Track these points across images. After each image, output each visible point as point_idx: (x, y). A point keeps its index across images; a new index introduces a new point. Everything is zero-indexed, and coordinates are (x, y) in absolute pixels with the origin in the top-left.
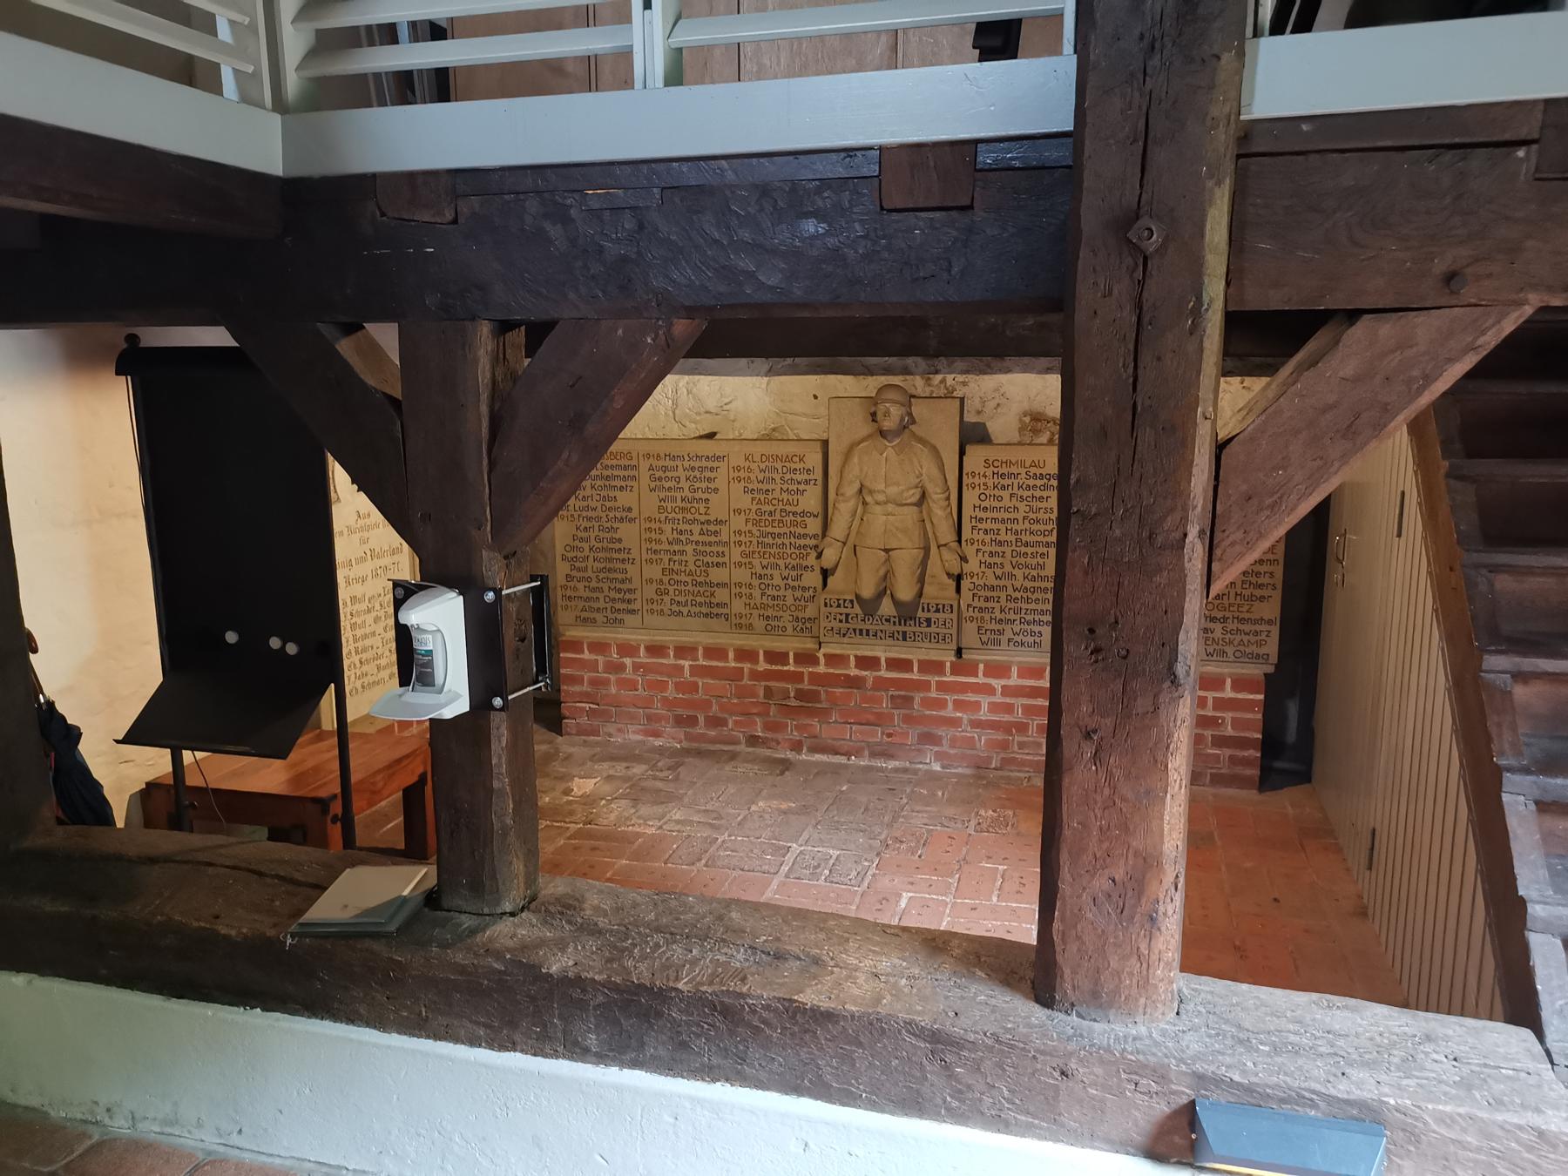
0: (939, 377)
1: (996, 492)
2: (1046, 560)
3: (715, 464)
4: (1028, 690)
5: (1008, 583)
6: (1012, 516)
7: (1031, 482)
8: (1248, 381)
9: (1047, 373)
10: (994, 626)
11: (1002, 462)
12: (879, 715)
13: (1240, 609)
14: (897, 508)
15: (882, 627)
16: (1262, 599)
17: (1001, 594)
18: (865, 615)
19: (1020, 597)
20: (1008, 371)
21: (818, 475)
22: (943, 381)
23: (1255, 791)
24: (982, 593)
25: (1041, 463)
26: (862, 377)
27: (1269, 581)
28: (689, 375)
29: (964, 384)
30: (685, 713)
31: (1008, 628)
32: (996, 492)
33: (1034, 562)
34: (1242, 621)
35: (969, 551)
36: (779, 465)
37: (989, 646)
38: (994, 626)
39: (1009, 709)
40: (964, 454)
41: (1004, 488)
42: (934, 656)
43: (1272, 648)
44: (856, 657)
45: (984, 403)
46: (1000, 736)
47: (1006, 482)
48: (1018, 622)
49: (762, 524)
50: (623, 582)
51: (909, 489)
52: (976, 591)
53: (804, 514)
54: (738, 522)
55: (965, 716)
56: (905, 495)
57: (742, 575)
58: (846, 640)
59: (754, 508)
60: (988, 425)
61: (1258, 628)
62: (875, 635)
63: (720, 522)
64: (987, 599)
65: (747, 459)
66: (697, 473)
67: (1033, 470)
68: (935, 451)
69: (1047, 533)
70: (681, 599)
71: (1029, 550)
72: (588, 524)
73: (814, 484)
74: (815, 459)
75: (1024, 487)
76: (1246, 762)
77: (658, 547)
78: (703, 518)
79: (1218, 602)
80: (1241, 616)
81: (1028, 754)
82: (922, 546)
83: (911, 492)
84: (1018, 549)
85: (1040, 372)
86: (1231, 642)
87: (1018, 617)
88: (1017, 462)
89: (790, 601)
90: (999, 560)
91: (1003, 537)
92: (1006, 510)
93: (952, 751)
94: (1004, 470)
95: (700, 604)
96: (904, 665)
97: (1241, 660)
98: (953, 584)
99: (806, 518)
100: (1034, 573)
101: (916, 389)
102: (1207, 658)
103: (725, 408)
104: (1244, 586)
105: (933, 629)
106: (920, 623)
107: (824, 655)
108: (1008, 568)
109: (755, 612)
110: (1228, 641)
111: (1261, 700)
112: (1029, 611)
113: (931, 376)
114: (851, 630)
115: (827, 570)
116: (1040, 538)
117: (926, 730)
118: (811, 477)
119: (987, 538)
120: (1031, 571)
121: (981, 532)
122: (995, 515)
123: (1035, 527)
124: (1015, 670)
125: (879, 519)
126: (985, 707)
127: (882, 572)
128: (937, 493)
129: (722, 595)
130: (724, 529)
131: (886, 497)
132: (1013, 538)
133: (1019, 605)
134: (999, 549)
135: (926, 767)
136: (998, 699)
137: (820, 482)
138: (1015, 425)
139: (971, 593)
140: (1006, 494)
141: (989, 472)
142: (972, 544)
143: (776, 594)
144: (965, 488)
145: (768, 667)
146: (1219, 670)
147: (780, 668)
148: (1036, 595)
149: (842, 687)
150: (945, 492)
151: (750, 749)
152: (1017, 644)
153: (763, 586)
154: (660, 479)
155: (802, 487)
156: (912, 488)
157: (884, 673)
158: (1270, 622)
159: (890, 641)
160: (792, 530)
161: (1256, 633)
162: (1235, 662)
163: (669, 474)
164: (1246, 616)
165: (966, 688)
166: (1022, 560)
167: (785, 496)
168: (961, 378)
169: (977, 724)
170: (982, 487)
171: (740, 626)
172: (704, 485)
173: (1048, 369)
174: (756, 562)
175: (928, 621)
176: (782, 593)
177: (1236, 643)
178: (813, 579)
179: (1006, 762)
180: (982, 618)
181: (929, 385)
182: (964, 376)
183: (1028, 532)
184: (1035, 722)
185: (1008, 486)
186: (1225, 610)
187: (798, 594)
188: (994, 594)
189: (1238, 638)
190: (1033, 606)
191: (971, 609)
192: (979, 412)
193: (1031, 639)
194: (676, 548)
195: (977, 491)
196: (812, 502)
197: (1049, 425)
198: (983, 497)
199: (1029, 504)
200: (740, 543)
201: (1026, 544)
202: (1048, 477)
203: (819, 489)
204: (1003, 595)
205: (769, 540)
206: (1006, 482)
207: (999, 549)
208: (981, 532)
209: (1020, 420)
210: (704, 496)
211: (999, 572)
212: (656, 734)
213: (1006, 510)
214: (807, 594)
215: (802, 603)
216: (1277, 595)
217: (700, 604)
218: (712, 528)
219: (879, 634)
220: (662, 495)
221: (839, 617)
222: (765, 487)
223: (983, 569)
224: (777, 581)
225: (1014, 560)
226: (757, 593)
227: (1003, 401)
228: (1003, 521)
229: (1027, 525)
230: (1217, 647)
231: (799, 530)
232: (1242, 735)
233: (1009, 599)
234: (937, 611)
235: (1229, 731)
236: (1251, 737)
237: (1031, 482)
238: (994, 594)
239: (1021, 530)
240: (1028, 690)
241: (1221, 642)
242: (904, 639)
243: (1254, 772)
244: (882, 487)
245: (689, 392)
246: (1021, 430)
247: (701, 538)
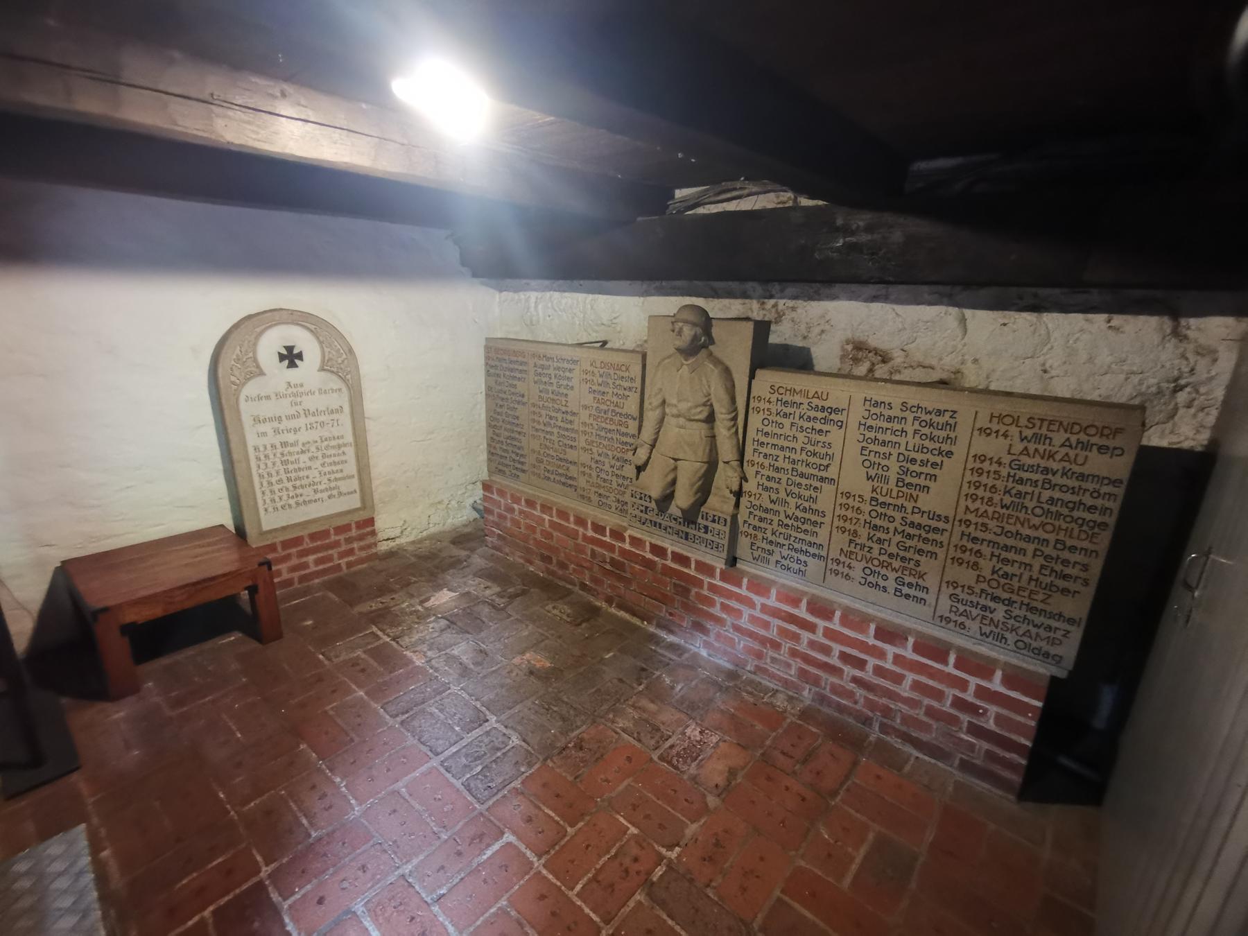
0: (772, 302)
1: (779, 419)
2: (818, 494)
3: (572, 366)
4: (783, 614)
5: (781, 509)
6: (791, 445)
7: (812, 414)
8: (1118, 320)
9: (872, 301)
10: (764, 545)
11: (787, 390)
12: (665, 596)
13: (1033, 596)
14: (687, 423)
15: (671, 525)
16: (1065, 591)
17: (773, 517)
19: (790, 524)
20: (833, 297)
21: (638, 384)
22: (775, 306)
23: (1012, 797)
24: (757, 513)
25: (825, 394)
27: (1082, 574)
28: (593, 294)
29: (793, 309)
30: (546, 553)
31: (777, 550)
32: (779, 419)
33: (807, 494)
34: (1031, 609)
35: (750, 471)
36: (612, 372)
37: (759, 563)
38: (764, 545)
39: (766, 625)
40: (754, 378)
41: (785, 415)
42: (708, 560)
43: (1069, 649)
44: (650, 543)
45: (809, 328)
46: (757, 646)
47: (788, 410)
48: (787, 547)
49: (608, 422)
50: (519, 448)
51: (697, 406)
52: (752, 510)
53: (627, 416)
54: (584, 416)
55: (729, 619)
56: (694, 411)
57: (585, 458)
58: (644, 527)
59: (595, 405)
60: (813, 350)
61: (1054, 624)
62: (665, 529)
63: (574, 414)
64: (761, 520)
65: (592, 365)
66: (561, 373)
67: (815, 402)
68: (727, 372)
69: (822, 468)
70: (550, 468)
71: (804, 481)
72: (501, 403)
74: (636, 370)
75: (805, 417)
76: (1019, 728)
77: (538, 427)
78: (564, 409)
79: (1006, 581)
80: (1034, 604)
81: (778, 670)
82: (705, 460)
83: (699, 409)
84: (793, 478)
85: (866, 301)
86: (1013, 630)
87: (786, 542)
88: (801, 391)
89: (614, 485)
90: (775, 486)
91: (780, 464)
92: (786, 438)
93: (717, 644)
94: (787, 398)
95: (560, 475)
96: (684, 560)
97: (1022, 651)
98: (733, 499)
100: (806, 505)
101: (752, 312)
102: (979, 637)
103: (615, 321)
104: (1043, 571)
105: (709, 536)
106: (699, 528)
107: (629, 536)
108: (782, 495)
109: (594, 489)
110: (1010, 626)
111: (1038, 707)
112: (797, 540)
113: (766, 300)
114: (648, 521)
115: (640, 467)
116: (815, 472)
117: (697, 619)
118: (634, 385)
119: (766, 463)
120: (803, 502)
121: (761, 455)
122: (775, 441)
123: (812, 460)
124: (774, 592)
125: (672, 431)
126: (745, 616)
127: (670, 477)
128: (722, 414)
129: (573, 471)
130: (576, 419)
131: (678, 411)
132: (790, 467)
133: (789, 531)
134: (776, 475)
135: (696, 650)
136: (757, 613)
137: (639, 390)
138: (837, 352)
140: (787, 422)
141: (774, 398)
143: (606, 477)
144: (751, 411)
145: (594, 535)
146: (993, 654)
147: (599, 537)
148: (804, 527)
149: (640, 565)
150: (732, 412)
151: (581, 592)
152: (783, 567)
153: (598, 470)
154: (540, 374)
155: (627, 393)
156: (699, 406)
157: (669, 563)
158: (1071, 621)
159: (675, 537)
160: (619, 428)
161: (1049, 628)
162: (1015, 652)
163: (545, 371)
164: (1040, 606)
165: (730, 595)
166: (796, 490)
167: (615, 399)
168: (791, 303)
169: (737, 628)
170: (766, 412)
171: (583, 497)
172: (565, 382)
173: (874, 297)
174: (595, 450)
175: (706, 528)
176: (609, 478)
177: (1021, 632)
178: (630, 471)
179: (759, 670)
180: (756, 536)
181: (763, 309)
182: (794, 301)
183: (804, 464)
184: (788, 645)
185: (790, 414)
186: (1012, 592)
187: (620, 481)
188: (768, 516)
189: (1024, 627)
190: (802, 536)
191: (746, 525)
192: (805, 338)
193: (796, 566)
194: (549, 429)
197: (870, 354)
198: (766, 422)
199: (808, 435)
200: (585, 433)
201: (802, 475)
202: (829, 410)
203: (637, 396)
204: (776, 519)
205: (603, 434)
206: (788, 410)
207: (776, 475)
208: (761, 455)
209: (843, 349)
210: (565, 391)
211: (774, 497)
212: (531, 563)
213: (786, 438)
216: (1088, 593)
217: (560, 475)
218: (569, 417)
219: (668, 529)
220: (542, 387)
221: (641, 508)
222: (602, 389)
223: (760, 490)
224: (607, 467)
225: (789, 489)
226: (594, 474)
227: (827, 327)
228: (782, 449)
229: (804, 456)
230: (995, 630)
231: (623, 430)
232: (1007, 734)
233: (781, 524)
234: (714, 521)
235: (991, 725)
236: (1018, 741)
237: (812, 414)
238: (768, 516)
240: (783, 614)
241: (1001, 626)
242: (687, 539)
243: (1016, 778)
244: (674, 401)
245: (592, 308)
246: (843, 358)
247: (562, 424)
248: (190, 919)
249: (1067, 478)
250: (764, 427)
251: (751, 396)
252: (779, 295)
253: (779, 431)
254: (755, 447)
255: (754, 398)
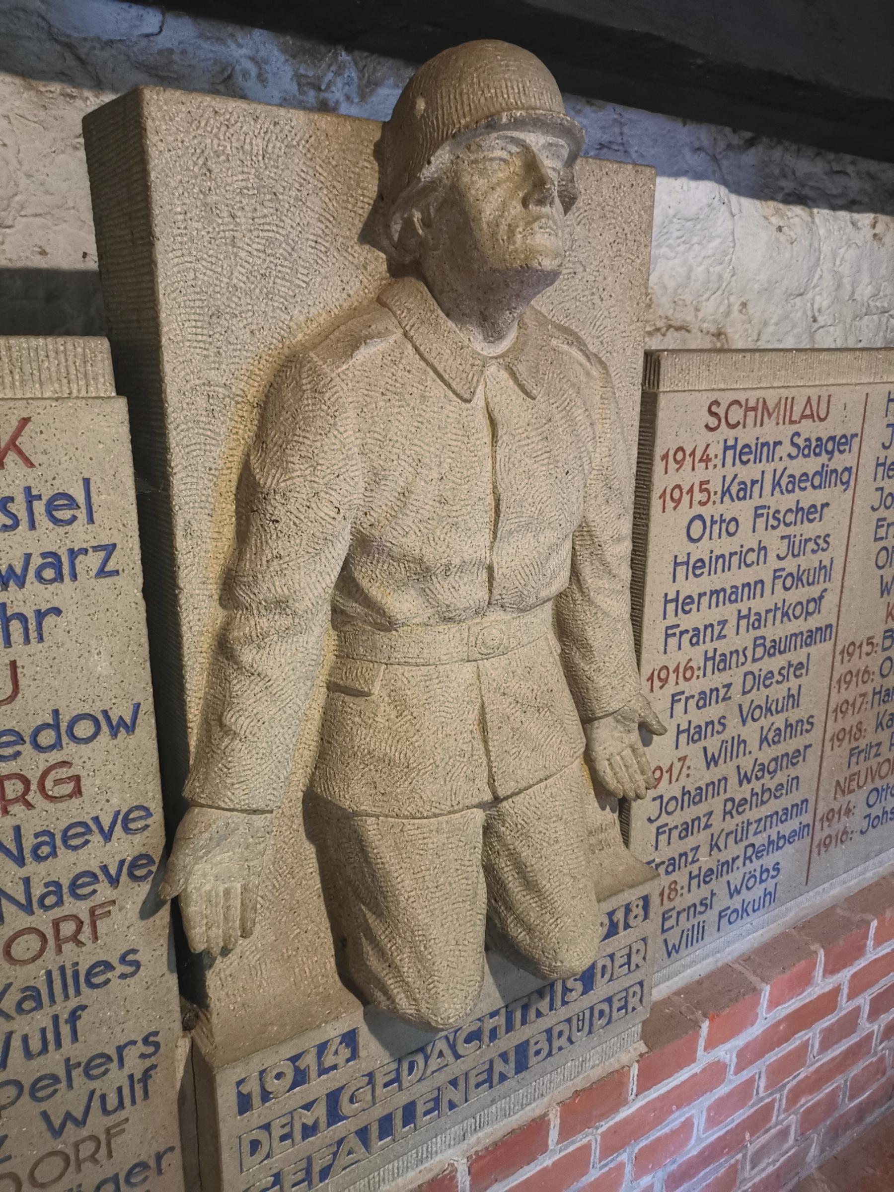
18: (400, 1061)
26: (56, 87)
73: (102, 573)
99: (70, 750)
114: (354, 1141)
139: (653, 828)
142: (664, 681)
144: (656, 504)
173: (602, 146)
183: (779, 614)
185: (754, 482)
195: (685, 512)
196: (102, 666)
203: (664, 442)
214: (116, 1077)
215: (97, 1123)
228: (733, 595)
233: (735, 807)
239: (767, 612)
248: (877, 928)
249: (720, 850)
250: (692, 547)
251: (659, 452)
252: (354, 110)
253: (725, 545)
254: (671, 620)
255: (665, 457)
